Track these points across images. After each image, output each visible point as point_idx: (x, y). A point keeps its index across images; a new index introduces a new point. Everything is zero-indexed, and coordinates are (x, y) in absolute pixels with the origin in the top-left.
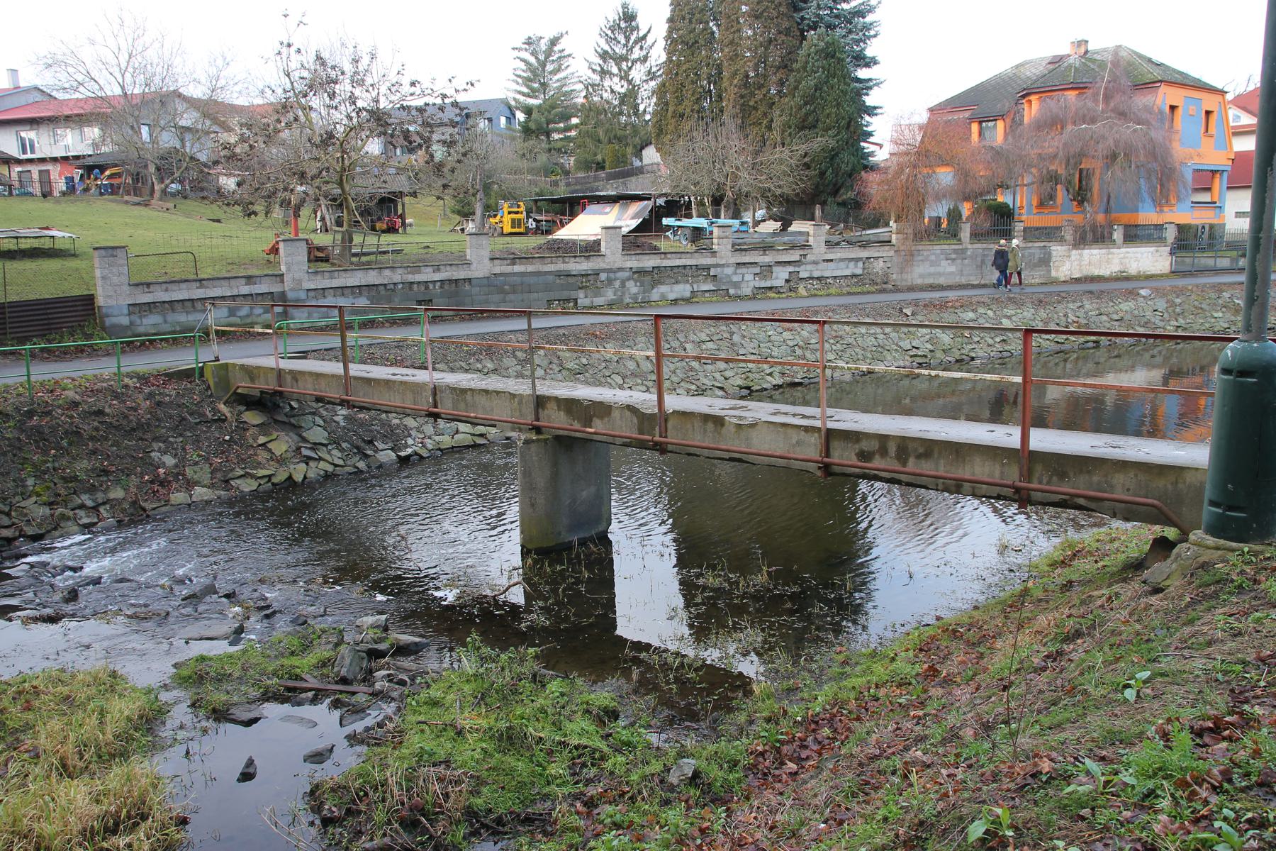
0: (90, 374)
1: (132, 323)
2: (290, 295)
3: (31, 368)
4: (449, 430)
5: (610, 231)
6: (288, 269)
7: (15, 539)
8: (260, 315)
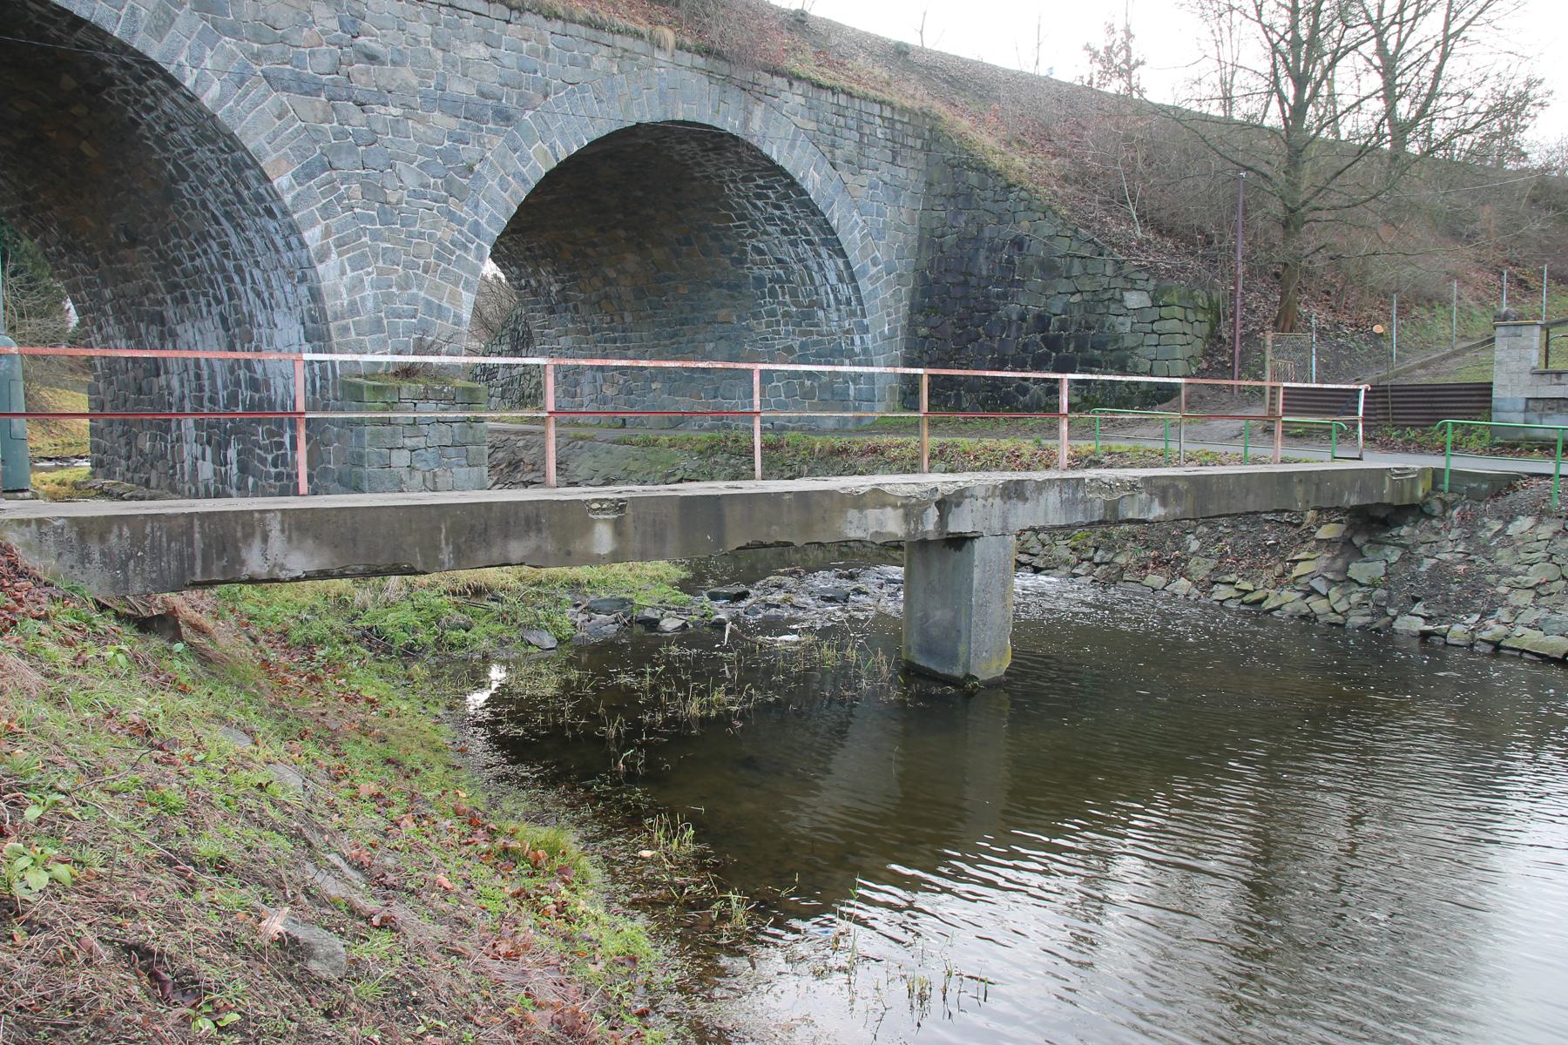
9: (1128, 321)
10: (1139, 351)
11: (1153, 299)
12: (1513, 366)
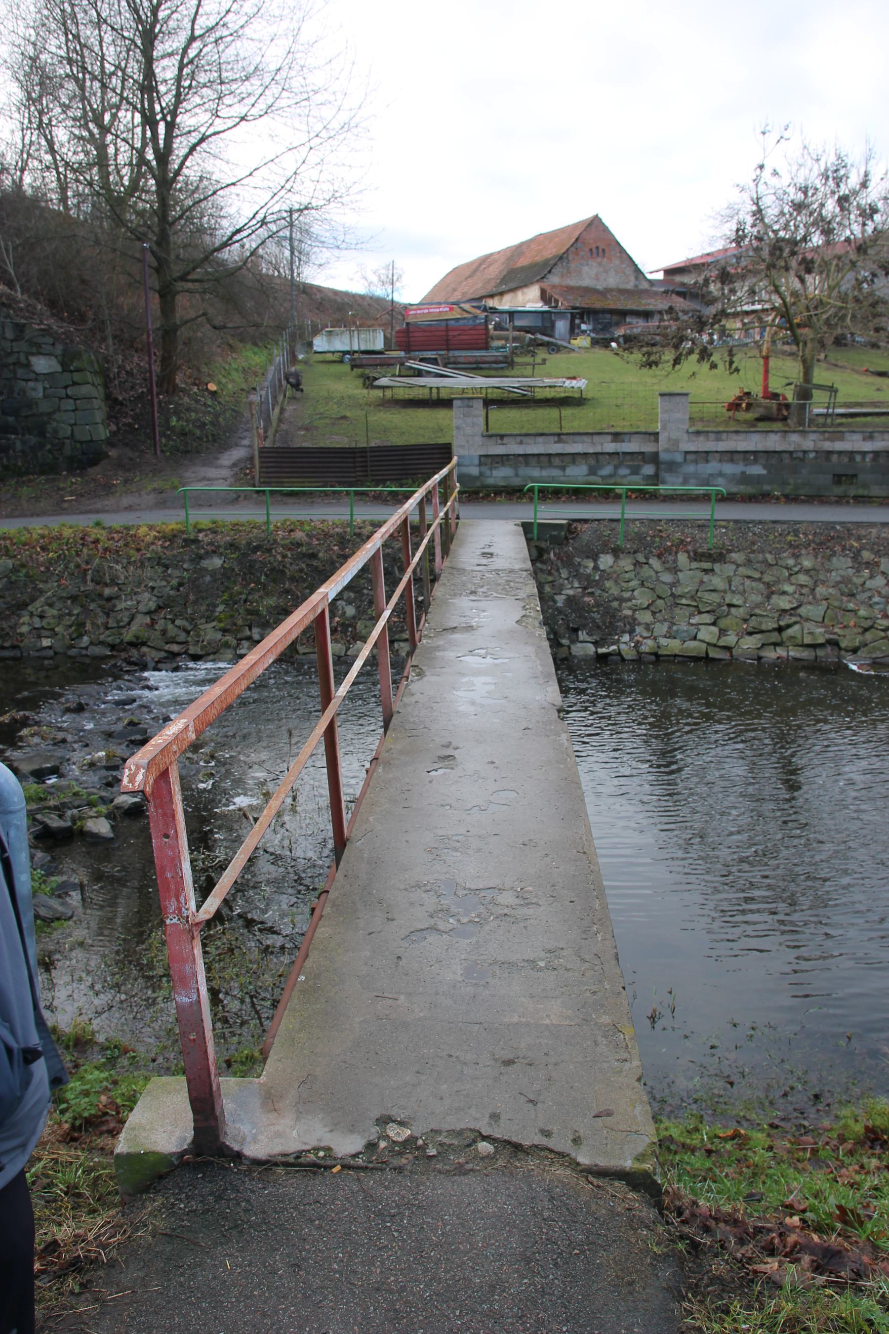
0: (294, 518)
1: (481, 474)
2: (663, 456)
3: (355, 509)
4: (685, 634)
5: (666, 398)
6: (664, 427)
7: (179, 654)
8: (625, 476)
9: (40, 387)
10: (57, 416)
11: (63, 364)
12: (469, 430)
